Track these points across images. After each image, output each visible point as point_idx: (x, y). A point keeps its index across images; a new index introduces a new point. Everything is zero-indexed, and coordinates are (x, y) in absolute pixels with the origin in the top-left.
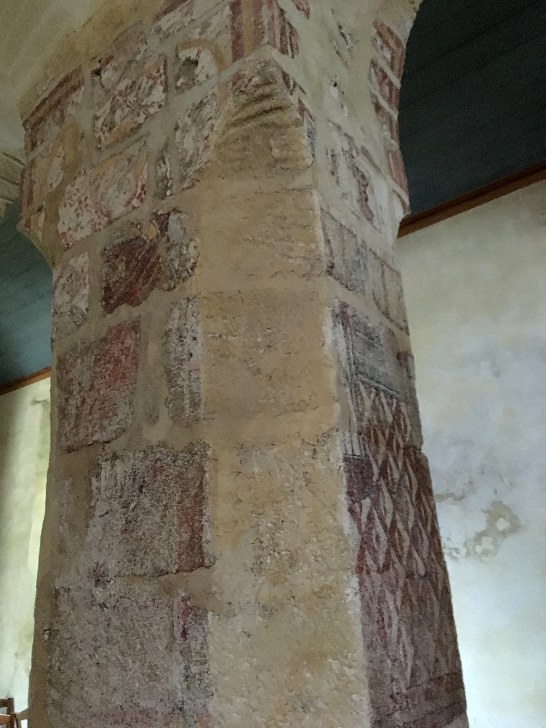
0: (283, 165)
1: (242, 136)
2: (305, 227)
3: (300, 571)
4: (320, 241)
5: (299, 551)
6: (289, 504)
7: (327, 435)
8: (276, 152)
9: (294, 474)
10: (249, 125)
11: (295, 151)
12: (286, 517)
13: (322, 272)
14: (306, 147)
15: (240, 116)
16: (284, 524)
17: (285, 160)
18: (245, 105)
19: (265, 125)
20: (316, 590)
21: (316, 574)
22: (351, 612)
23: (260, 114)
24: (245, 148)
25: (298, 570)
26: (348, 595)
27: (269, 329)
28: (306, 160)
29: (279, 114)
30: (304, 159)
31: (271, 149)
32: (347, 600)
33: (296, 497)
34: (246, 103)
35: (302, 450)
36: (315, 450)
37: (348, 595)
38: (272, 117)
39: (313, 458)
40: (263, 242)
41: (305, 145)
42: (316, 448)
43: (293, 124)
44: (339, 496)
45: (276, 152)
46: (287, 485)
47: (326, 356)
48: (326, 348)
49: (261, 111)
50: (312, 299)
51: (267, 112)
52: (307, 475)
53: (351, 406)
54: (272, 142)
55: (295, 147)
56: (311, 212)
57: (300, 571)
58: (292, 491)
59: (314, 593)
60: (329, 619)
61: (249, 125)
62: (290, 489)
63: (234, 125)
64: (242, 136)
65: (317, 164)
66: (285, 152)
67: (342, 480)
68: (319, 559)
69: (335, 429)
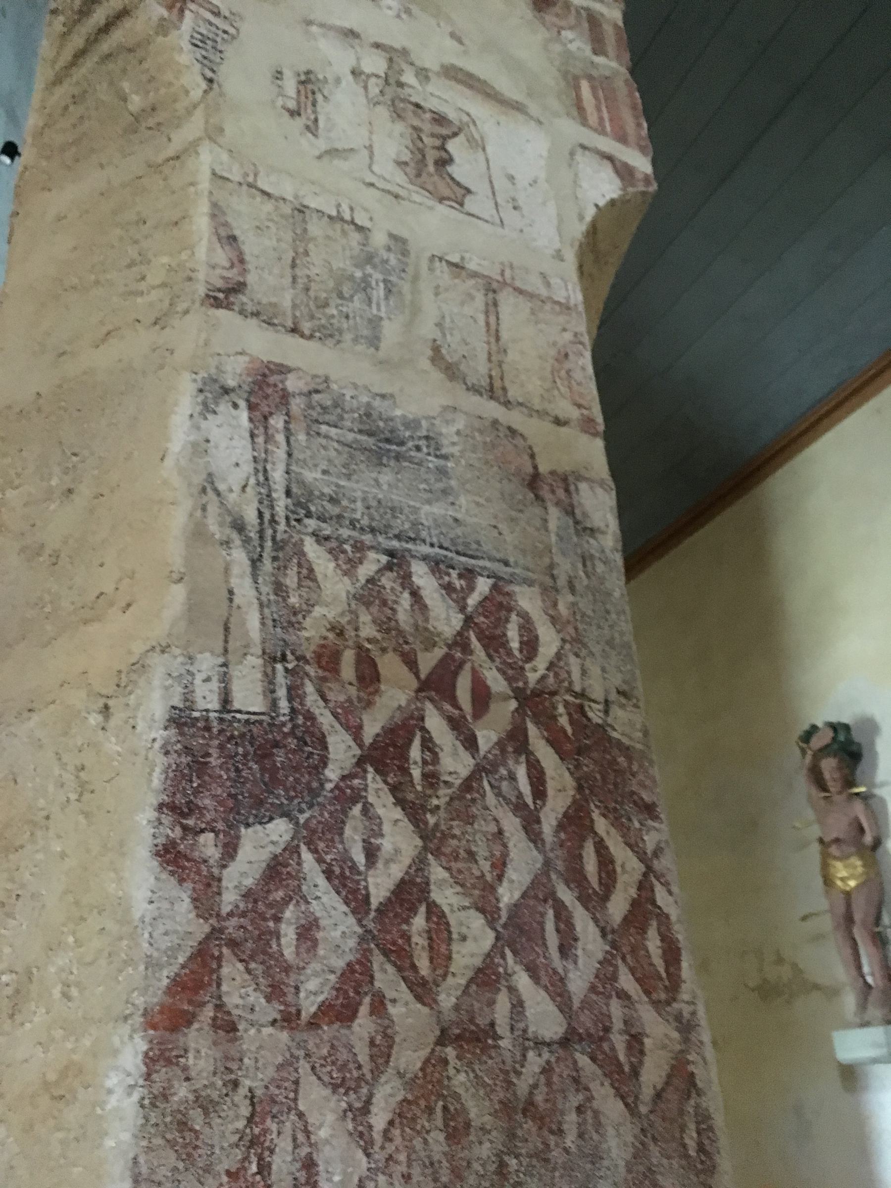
0: (151, 122)
1: (74, 97)
2: (176, 223)
3: (28, 1025)
4: (201, 239)
5: (34, 970)
6: (37, 851)
7: (140, 667)
8: (136, 102)
9: (61, 776)
10: (83, 70)
11: (170, 84)
12: (23, 886)
13: (193, 302)
14: (187, 67)
15: (61, 63)
16: (20, 903)
17: (153, 109)
18: (64, 36)
19: (108, 57)
20: (52, 1077)
21: (58, 1033)
22: (110, 1143)
23: (96, 40)
24: (82, 117)
25: (22, 1024)
26: (110, 1092)
27: (75, 455)
28: (192, 93)
29: (127, 23)
30: (187, 92)
31: (125, 100)
32: (109, 1107)
33: (51, 833)
34: (65, 30)
35: (84, 714)
36: (106, 707)
37: (110, 1092)
38: (117, 36)
39: (103, 729)
40: (97, 282)
41: (188, 63)
42: (111, 703)
43: (157, 33)
44: (137, 818)
45: (136, 102)
46: (42, 802)
47: (165, 482)
48: (169, 462)
49: (95, 31)
50: (162, 367)
51: (106, 29)
52: (82, 774)
53: (245, 590)
54: (126, 86)
55: (169, 76)
56: (192, 189)
57: (28, 1025)
58: (47, 818)
59: (46, 1085)
60: (62, 1161)
61: (79, 73)
62: (45, 813)
63: (57, 81)
64: (74, 97)
65: (222, 94)
66: (151, 94)
67: (150, 774)
68: (74, 991)
69: (158, 649)
